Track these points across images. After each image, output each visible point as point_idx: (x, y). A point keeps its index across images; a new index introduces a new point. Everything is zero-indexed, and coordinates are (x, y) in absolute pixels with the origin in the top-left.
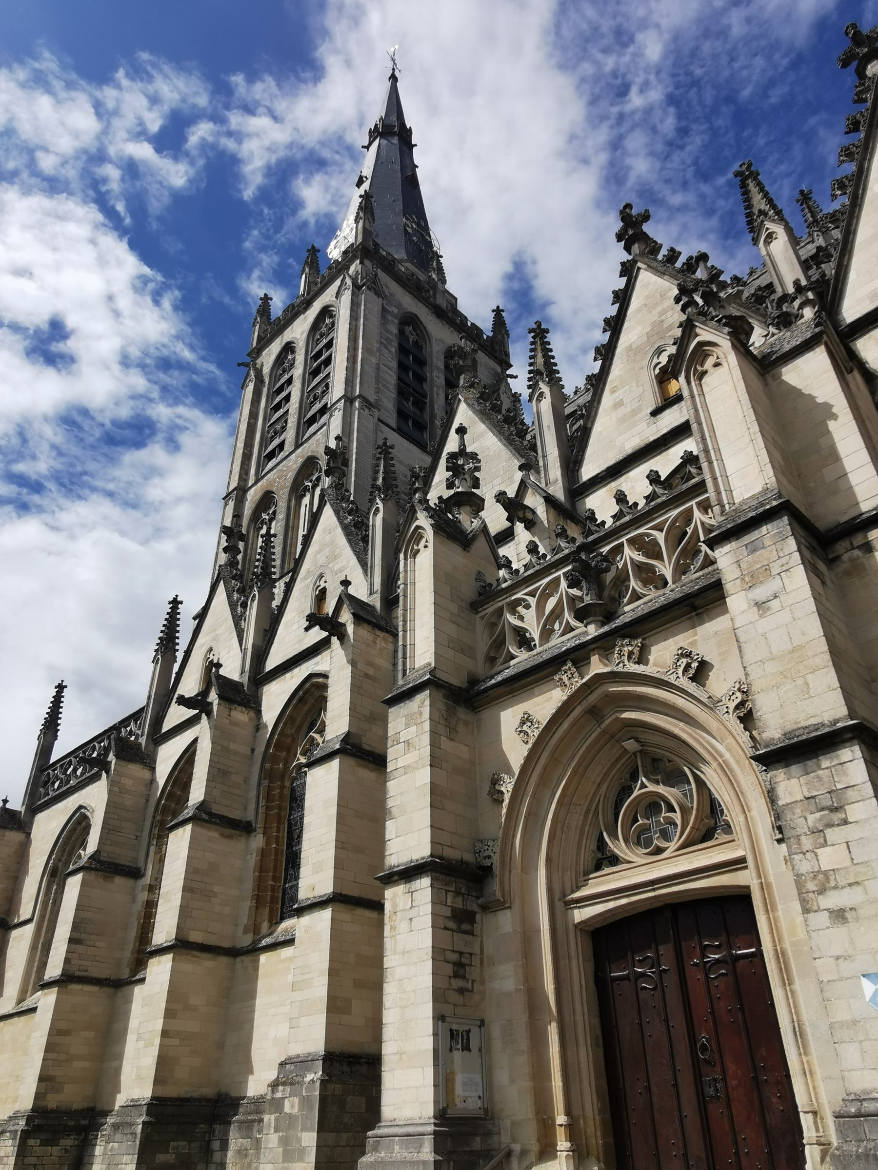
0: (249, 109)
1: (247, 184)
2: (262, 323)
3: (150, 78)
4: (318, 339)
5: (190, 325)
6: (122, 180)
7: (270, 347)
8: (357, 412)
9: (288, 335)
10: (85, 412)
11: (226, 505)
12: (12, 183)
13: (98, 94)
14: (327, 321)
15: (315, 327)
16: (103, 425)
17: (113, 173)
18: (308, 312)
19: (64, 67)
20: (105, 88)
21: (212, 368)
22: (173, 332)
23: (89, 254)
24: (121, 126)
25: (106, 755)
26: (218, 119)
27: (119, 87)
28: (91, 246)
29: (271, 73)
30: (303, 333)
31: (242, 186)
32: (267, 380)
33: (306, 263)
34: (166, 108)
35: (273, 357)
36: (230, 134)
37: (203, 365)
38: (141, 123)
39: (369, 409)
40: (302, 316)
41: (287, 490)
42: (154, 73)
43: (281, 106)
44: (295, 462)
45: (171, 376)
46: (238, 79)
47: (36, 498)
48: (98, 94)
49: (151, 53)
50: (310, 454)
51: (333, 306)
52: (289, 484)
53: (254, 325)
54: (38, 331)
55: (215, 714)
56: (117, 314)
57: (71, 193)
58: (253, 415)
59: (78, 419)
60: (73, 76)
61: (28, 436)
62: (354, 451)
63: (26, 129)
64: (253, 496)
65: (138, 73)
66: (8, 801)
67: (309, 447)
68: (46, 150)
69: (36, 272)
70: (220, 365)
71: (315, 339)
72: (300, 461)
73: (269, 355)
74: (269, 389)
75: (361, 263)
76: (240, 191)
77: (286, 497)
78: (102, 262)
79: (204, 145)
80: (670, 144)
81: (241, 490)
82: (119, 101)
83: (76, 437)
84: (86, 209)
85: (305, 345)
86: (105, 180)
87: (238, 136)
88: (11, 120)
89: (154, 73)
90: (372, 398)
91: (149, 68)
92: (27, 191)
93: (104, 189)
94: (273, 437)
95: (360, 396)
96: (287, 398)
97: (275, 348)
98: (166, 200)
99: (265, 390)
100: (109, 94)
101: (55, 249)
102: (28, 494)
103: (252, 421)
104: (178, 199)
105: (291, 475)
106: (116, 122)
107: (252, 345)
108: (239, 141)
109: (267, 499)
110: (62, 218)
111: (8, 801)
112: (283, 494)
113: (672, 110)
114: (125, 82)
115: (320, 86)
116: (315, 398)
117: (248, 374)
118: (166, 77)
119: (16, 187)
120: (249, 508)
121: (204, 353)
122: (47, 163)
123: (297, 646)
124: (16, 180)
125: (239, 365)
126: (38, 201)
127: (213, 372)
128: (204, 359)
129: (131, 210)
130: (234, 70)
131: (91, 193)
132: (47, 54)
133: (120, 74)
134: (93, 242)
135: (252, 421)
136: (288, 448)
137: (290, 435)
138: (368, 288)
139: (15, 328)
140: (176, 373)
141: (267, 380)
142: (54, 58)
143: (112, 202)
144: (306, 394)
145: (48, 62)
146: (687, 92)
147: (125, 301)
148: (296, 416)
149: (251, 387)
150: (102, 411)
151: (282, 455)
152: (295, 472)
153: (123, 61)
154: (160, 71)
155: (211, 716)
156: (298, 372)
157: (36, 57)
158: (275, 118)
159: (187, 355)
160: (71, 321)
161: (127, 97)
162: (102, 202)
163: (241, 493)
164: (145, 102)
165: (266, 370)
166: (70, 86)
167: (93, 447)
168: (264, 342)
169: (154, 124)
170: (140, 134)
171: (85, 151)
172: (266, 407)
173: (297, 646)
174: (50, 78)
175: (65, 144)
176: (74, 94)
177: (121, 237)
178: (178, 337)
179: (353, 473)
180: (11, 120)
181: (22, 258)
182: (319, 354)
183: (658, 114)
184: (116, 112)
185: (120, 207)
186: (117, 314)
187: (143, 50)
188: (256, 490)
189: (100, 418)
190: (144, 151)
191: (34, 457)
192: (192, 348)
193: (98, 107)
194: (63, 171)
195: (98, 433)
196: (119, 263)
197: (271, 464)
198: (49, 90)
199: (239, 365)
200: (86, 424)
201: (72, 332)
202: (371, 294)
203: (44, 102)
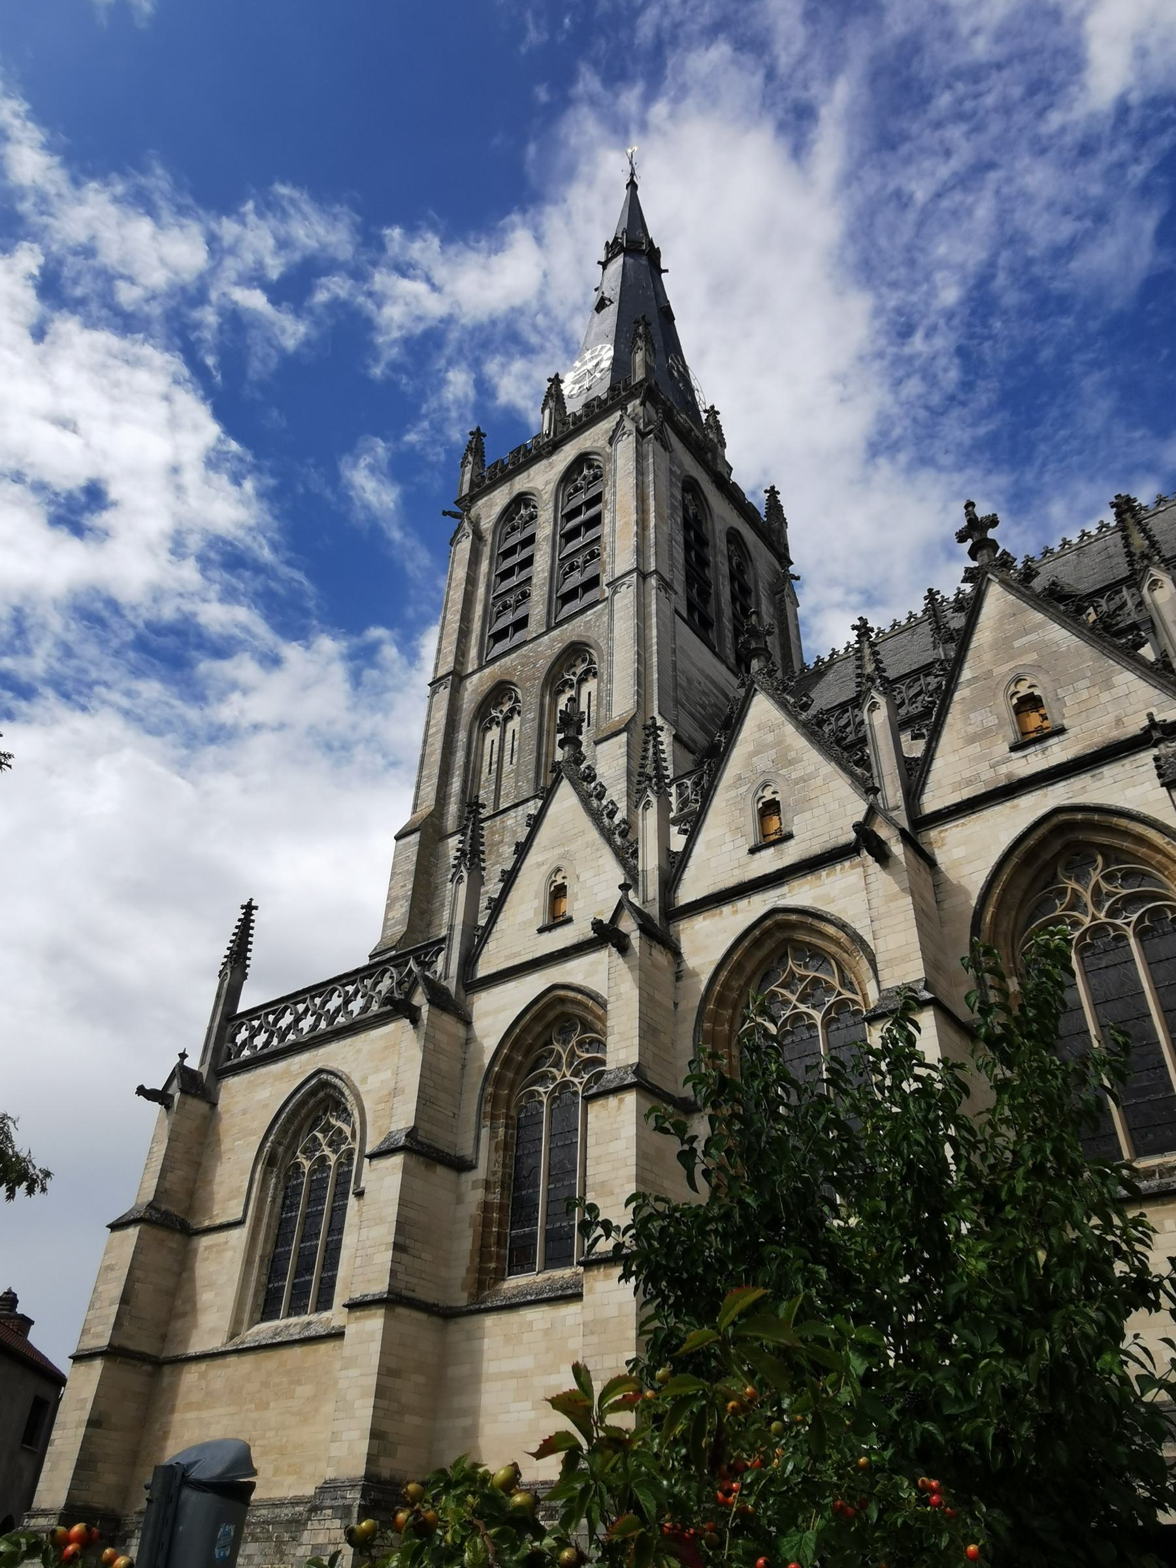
0: (404, 269)
1: (376, 360)
2: (475, 464)
3: (284, 216)
4: (571, 494)
5: (276, 517)
6: (220, 329)
7: (492, 496)
8: (654, 592)
9: (521, 483)
10: (113, 605)
11: (434, 693)
12: (74, 312)
13: (213, 225)
14: (585, 472)
15: (508, 513)
16: (133, 626)
17: (209, 317)
18: (554, 458)
19: (178, 186)
20: (224, 220)
21: (298, 575)
22: (252, 522)
23: (160, 410)
24: (231, 267)
25: (410, 994)
26: (359, 275)
27: (242, 221)
28: (165, 404)
29: (436, 231)
30: (547, 483)
31: (370, 361)
32: (489, 538)
33: (469, 449)
34: (297, 257)
35: (497, 510)
36: (370, 294)
37: (285, 571)
38: (260, 265)
39: (666, 592)
40: (544, 462)
41: (538, 683)
42: (292, 211)
43: (440, 274)
44: (551, 647)
45: (239, 577)
46: (395, 234)
47: (23, 705)
48: (213, 225)
49: (295, 185)
50: (574, 638)
51: (599, 454)
52: (541, 674)
53: (463, 465)
54: (70, 496)
55: (637, 950)
56: (179, 489)
57: (150, 336)
58: (471, 581)
59: (106, 614)
60: (189, 201)
61: (27, 624)
62: (655, 640)
63: (110, 255)
64: (475, 686)
65: (269, 207)
66: (186, 1056)
67: (573, 630)
68: (131, 280)
69: (82, 424)
70: (309, 574)
71: (567, 493)
72: (558, 647)
73: (491, 506)
74: (492, 550)
75: (643, 404)
76: (367, 367)
77: (536, 690)
78: (174, 423)
79: (336, 305)
80: (952, 398)
81: (457, 677)
82: (238, 240)
83: (96, 636)
84: (167, 356)
85: (553, 498)
86: (198, 326)
87: (380, 300)
88: (93, 238)
89: (292, 211)
90: (667, 576)
91: (285, 203)
92: (91, 324)
93: (193, 337)
94: (500, 612)
95: (656, 572)
96: (528, 562)
97: (500, 498)
98: (273, 364)
99: (487, 551)
100: (228, 229)
101: (114, 399)
102: (15, 698)
103: (470, 587)
104: (290, 364)
105: (543, 664)
106: (229, 262)
107: (461, 490)
108: (380, 306)
109: (501, 690)
110: (134, 363)
111: (186, 1056)
112: (532, 686)
113: (957, 361)
114: (252, 218)
115: (494, 259)
116: (506, 607)
117: (460, 526)
118: (305, 217)
119: (77, 318)
120: (471, 701)
121: (289, 555)
122: (127, 295)
123: (736, 872)
124: (80, 309)
125: (445, 513)
126: (104, 338)
127: (301, 583)
128: (289, 563)
129: (222, 366)
130: (390, 224)
131: (177, 342)
132: (159, 171)
133: (250, 206)
134: (167, 398)
135: (470, 587)
136: (534, 628)
137: (537, 609)
138: (656, 438)
139: (40, 487)
140: (247, 574)
141: (489, 538)
142: (168, 176)
143: (202, 352)
144: (491, 600)
145: (159, 180)
146: (980, 344)
147: (192, 476)
148: (546, 589)
149: (465, 545)
150: (133, 608)
151: (519, 636)
152: (551, 660)
153: (253, 191)
154: (299, 209)
155: (629, 952)
156: (544, 529)
157: (144, 170)
158: (435, 288)
159: (266, 554)
160: (114, 492)
161: (250, 236)
162: (190, 354)
163: (457, 680)
164: (271, 242)
165: (487, 524)
166: (182, 211)
167: (117, 653)
168: (480, 488)
169: (275, 268)
170: (255, 278)
171: (183, 289)
172: (489, 573)
173: (736, 872)
174: (156, 197)
175: (158, 278)
176: (185, 221)
177: (204, 399)
178: (259, 529)
179: (655, 669)
180: (93, 238)
181: (67, 405)
182: (511, 552)
183: (942, 362)
184: (232, 251)
185: (210, 361)
186: (179, 489)
187: (283, 183)
188: (481, 678)
189: (131, 617)
190: (255, 300)
191: (28, 652)
192: (275, 547)
193: (212, 241)
194: (146, 308)
195: (130, 636)
196: (196, 428)
197: (500, 647)
198: (151, 211)
199: (445, 513)
200: (113, 621)
201: (115, 504)
202: (658, 445)
203: (143, 228)
